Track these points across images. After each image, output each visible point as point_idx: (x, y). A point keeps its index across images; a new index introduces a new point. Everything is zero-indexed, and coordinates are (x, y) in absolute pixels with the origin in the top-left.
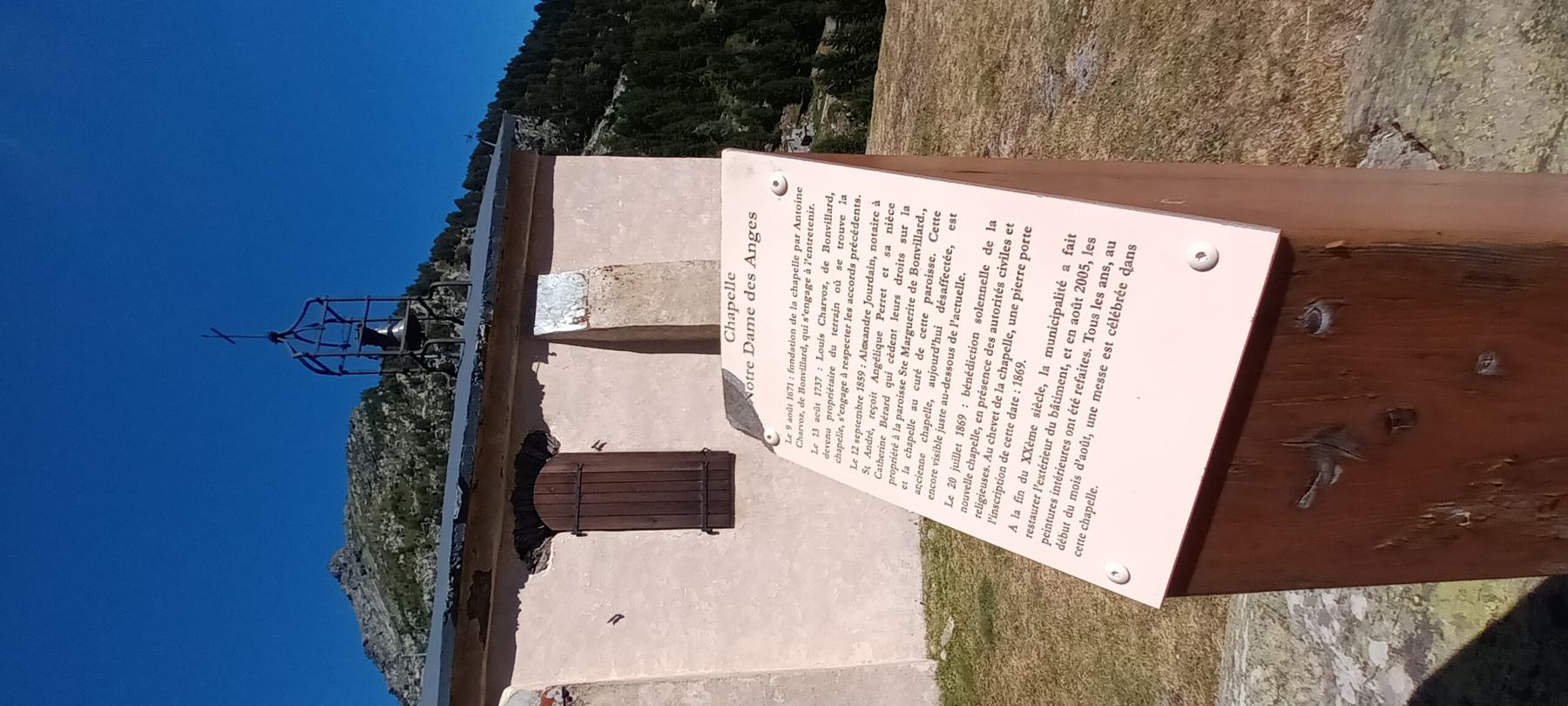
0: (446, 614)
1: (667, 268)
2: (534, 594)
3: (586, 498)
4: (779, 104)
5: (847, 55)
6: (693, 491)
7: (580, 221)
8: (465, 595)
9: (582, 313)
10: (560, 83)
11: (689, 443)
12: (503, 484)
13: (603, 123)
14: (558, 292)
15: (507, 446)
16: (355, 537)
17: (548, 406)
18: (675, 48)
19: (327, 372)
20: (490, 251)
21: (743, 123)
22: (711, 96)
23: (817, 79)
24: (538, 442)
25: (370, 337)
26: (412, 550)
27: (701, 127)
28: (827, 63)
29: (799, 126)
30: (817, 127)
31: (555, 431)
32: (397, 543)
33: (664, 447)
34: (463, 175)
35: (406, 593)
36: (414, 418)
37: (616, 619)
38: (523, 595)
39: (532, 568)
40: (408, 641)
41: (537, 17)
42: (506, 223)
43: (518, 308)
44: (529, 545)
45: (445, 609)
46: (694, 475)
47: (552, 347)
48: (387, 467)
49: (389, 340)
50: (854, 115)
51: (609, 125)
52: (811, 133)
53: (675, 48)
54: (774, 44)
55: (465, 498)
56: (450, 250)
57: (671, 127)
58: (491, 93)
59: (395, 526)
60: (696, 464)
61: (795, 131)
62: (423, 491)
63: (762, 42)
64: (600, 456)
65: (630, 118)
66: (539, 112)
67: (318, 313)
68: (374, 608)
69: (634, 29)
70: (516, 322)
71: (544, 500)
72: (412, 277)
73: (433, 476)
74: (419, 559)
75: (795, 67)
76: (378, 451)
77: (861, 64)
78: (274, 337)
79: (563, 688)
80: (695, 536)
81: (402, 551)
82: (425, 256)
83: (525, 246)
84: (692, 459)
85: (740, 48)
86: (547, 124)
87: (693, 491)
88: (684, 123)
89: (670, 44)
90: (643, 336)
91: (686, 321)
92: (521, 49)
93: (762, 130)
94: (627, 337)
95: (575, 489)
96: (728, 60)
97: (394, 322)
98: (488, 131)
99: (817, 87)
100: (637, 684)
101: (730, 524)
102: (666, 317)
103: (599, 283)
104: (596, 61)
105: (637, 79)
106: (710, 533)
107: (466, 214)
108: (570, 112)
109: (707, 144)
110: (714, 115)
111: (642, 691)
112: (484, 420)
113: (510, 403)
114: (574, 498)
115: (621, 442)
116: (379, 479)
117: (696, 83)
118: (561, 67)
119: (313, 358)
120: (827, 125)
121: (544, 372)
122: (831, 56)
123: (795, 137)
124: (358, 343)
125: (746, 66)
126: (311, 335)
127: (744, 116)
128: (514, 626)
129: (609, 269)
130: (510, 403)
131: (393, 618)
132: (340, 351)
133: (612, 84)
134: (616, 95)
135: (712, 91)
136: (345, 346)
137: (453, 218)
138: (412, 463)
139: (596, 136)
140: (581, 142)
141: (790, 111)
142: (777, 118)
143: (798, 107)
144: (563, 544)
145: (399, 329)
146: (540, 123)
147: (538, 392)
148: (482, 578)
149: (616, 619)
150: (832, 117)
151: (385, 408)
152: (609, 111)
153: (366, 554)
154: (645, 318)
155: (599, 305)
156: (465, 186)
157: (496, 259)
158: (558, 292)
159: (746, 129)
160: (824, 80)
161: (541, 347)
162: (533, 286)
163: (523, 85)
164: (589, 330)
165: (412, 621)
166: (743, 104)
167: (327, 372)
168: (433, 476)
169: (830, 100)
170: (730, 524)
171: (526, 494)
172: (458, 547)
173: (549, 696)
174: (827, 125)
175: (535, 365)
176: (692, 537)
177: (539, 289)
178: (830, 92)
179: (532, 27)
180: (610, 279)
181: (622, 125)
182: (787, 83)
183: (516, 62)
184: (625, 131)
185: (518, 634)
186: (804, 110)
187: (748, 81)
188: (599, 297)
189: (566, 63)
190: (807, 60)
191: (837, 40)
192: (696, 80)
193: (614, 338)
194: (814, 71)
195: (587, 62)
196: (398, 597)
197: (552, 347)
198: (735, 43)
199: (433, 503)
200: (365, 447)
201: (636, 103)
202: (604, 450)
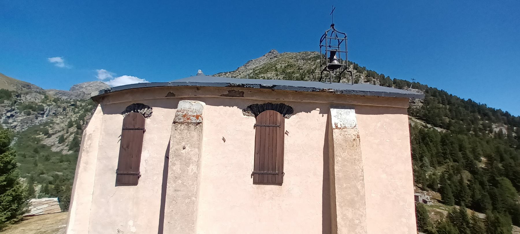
0: (229, 83)
1: (360, 160)
2: (236, 112)
3: (267, 128)
4: (440, 191)
5: (468, 223)
6: (268, 169)
7: (379, 125)
8: (236, 89)
9: (339, 126)
10: (439, 108)
11: (287, 168)
12: (274, 100)
13: (424, 124)
14: (348, 117)
15: (288, 101)
16: (281, 55)
17: (303, 114)
18: (460, 150)
19: (321, 42)
20: (364, 92)
21: (430, 176)
22: (440, 163)
23: (455, 208)
24: (288, 111)
25: (333, 53)
26: (276, 70)
27: (427, 160)
28: (463, 214)
29: (431, 199)
30: (431, 206)
31: (293, 118)
32: (278, 67)
33: (286, 157)
34: (399, 78)
35: (265, 70)
36: (315, 69)
37: (224, 140)
38: (235, 108)
39: (244, 110)
40: (251, 71)
41: (466, 99)
42: (376, 97)
43: (341, 103)
44: (254, 110)
45: (231, 83)
46: (274, 169)
47: (326, 116)
48: (301, 63)
49: (331, 59)
50: (439, 223)
51: (423, 126)
52: (428, 204)
53: (460, 150)
54: (468, 191)
55: (269, 87)
56: (370, 76)
57: (425, 148)
58: (432, 85)
59: (283, 66)
60: (279, 170)
61: (429, 197)
62: (293, 72)
63: (468, 186)
64: (283, 133)
65: (427, 134)
66: (426, 102)
67: (341, 37)
68: (261, 61)
69: (466, 135)
70: (335, 102)
71: (268, 113)
72: (361, 65)
73: (298, 75)
74: (274, 72)
75: (459, 199)
76: (306, 59)
77: (465, 229)
78: (333, 25)
79: (201, 122)
80: (251, 169)
81: (276, 68)
82: (368, 68)
83: (365, 104)
84: (280, 168)
85: (464, 176)
86: (421, 104)
87: (268, 169)
88: (427, 153)
89: (461, 148)
90: (330, 150)
91: (336, 168)
92: (451, 95)
93: (428, 183)
94: (330, 144)
95: (271, 125)
96: (458, 171)
97: (339, 61)
98: (416, 86)
99: (451, 208)
100: (199, 148)
101: (255, 183)
102: (338, 160)
103: (352, 133)
104: (450, 121)
105: (444, 140)
106: (252, 175)
107: (384, 81)
108: (427, 112)
109: (419, 162)
110: (432, 165)
111: (197, 150)
112: (298, 92)
113: (304, 101)
114: (268, 124)
115: (288, 141)
116: (297, 60)
117: (445, 158)
118: (446, 108)
119: (325, 37)
120: (433, 211)
121: (316, 112)
122: (466, 215)
123: (425, 196)
124: (331, 50)
125: (456, 178)
126: (334, 36)
127: (433, 177)
128: (225, 105)
129: (358, 137)
130: (304, 101)
131: (258, 67)
132: (328, 45)
133: (441, 127)
134: (436, 128)
135: (443, 164)
136: (330, 46)
137: (383, 76)
138: (302, 69)
139: (418, 121)
140: (415, 116)
141: (438, 196)
142: (434, 189)
143: (440, 199)
144: (252, 120)
145: (336, 62)
146: (422, 102)
147: (308, 111)
148: (242, 94)
149: (224, 140)
150: (437, 213)
151: (319, 61)
152: (429, 126)
153: (276, 59)
154: (338, 151)
155: (343, 133)
156: (395, 79)
157: (363, 94)
158: (348, 117)
159: (427, 177)
160: (455, 211)
161: (325, 111)
162: (350, 107)
163: (434, 95)
164: (332, 129)
165: (256, 72)
166: (438, 177)
167: (321, 42)
168: (298, 75)
169: (445, 213)
170: (255, 183)
171: (270, 108)
172: (252, 86)
173: (200, 118)
174: (433, 211)
175: (319, 109)
176: (251, 168)
177: (349, 110)
178: (449, 214)
179: (461, 98)
180: (354, 137)
181: (424, 131)
182: (451, 195)
183: (446, 94)
184: (421, 132)
185: (222, 106)
186: (439, 201)
187: (449, 179)
188: (346, 133)
189: (448, 111)
190: (463, 204)
191: (474, 218)
192: (447, 158)
193: (330, 138)
194: (458, 207)
195: (449, 118)
196: (263, 68)
197: (326, 116)
198: (466, 175)
199: (289, 77)
200: (307, 56)
201: (434, 135)
202: (285, 135)
